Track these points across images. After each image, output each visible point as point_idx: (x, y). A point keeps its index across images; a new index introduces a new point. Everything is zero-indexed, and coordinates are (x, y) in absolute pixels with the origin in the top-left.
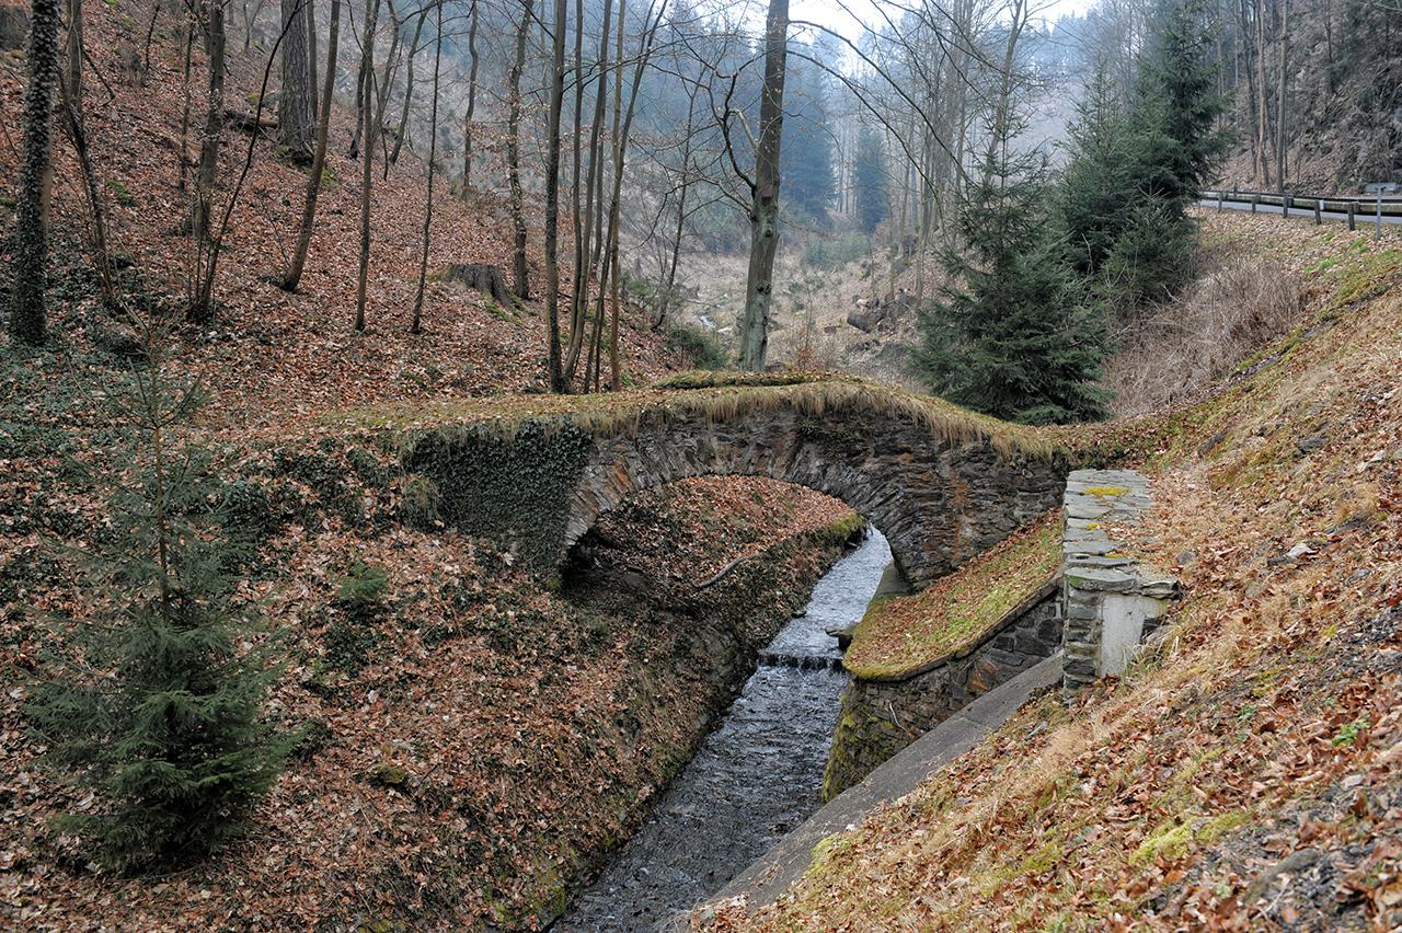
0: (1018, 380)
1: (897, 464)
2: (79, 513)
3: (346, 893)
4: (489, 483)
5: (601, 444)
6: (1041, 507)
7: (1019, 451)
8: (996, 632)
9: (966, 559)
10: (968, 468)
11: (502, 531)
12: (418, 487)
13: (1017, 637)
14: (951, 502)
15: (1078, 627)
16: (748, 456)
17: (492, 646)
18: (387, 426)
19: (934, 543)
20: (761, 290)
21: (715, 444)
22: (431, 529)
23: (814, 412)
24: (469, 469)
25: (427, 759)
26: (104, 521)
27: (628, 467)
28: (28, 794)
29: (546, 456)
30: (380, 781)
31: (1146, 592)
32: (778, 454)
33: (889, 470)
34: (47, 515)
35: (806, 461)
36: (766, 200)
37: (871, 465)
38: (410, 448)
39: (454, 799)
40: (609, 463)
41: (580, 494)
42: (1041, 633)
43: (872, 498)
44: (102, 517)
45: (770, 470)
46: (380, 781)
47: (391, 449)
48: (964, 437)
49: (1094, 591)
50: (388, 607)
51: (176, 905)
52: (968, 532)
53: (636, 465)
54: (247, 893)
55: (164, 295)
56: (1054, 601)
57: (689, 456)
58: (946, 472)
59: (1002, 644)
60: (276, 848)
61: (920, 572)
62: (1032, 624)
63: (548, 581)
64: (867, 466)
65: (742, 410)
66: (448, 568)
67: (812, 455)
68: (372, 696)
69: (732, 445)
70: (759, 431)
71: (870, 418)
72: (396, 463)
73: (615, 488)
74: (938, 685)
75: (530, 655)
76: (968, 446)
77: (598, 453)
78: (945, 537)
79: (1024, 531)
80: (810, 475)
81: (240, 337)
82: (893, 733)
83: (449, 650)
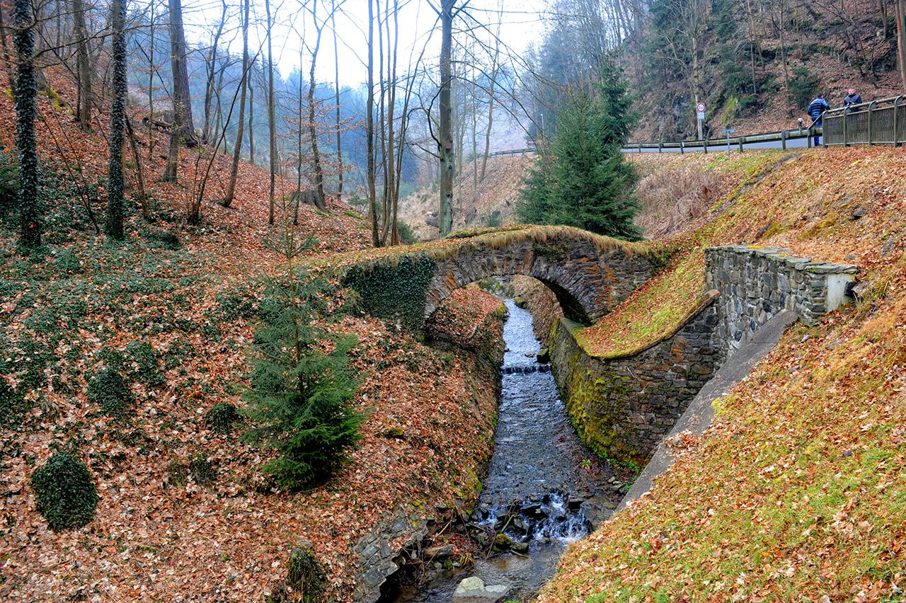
0: (605, 225)
1: (581, 263)
2: (192, 320)
3: (398, 488)
4: (385, 290)
5: (440, 265)
6: (644, 278)
7: (634, 252)
8: (685, 324)
9: (614, 306)
10: (612, 262)
11: (392, 314)
12: (350, 295)
13: (695, 325)
14: (606, 280)
15: (818, 291)
16: (512, 265)
17: (408, 369)
18: (329, 265)
19: (599, 300)
20: (448, 196)
21: (496, 260)
22: (361, 316)
23: (542, 241)
24: (375, 283)
25: (405, 423)
26: (206, 322)
27: (454, 275)
28: (226, 459)
29: (413, 273)
30: (391, 435)
31: (845, 272)
32: (526, 263)
33: (577, 267)
34: (176, 322)
35: (539, 265)
36: (448, 150)
37: (569, 264)
38: (344, 275)
39: (425, 441)
40: (444, 274)
41: (431, 291)
42: (707, 322)
43: (570, 281)
44: (204, 321)
45: (522, 271)
46: (391, 435)
47: (334, 277)
48: (610, 248)
49: (824, 273)
50: (355, 354)
51: (327, 502)
52: (614, 293)
53: (457, 274)
54: (356, 493)
55: (172, 211)
56: (712, 306)
57: (483, 267)
58: (603, 265)
59: (688, 330)
60: (358, 471)
61: (594, 315)
62: (702, 318)
63: (417, 337)
64: (567, 265)
65: (508, 242)
66: (375, 333)
67: (542, 262)
68: (364, 397)
69: (504, 260)
70: (516, 252)
71: (567, 242)
72: (337, 283)
73: (448, 287)
74: (655, 354)
75: (425, 372)
76: (611, 252)
77: (438, 270)
78: (604, 297)
79: (640, 290)
80: (541, 272)
81: (218, 231)
82: (630, 381)
83: (390, 372)
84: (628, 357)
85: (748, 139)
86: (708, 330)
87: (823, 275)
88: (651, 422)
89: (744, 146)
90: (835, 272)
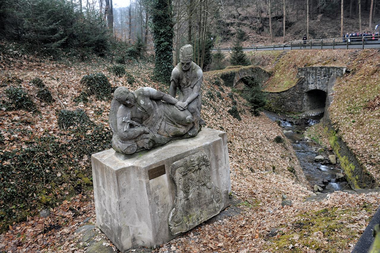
40: (237, 76)
84: (286, 91)
85: (258, 47)
86: (303, 84)
87: (343, 68)
88: (291, 104)
89: (257, 49)
90: (344, 68)
